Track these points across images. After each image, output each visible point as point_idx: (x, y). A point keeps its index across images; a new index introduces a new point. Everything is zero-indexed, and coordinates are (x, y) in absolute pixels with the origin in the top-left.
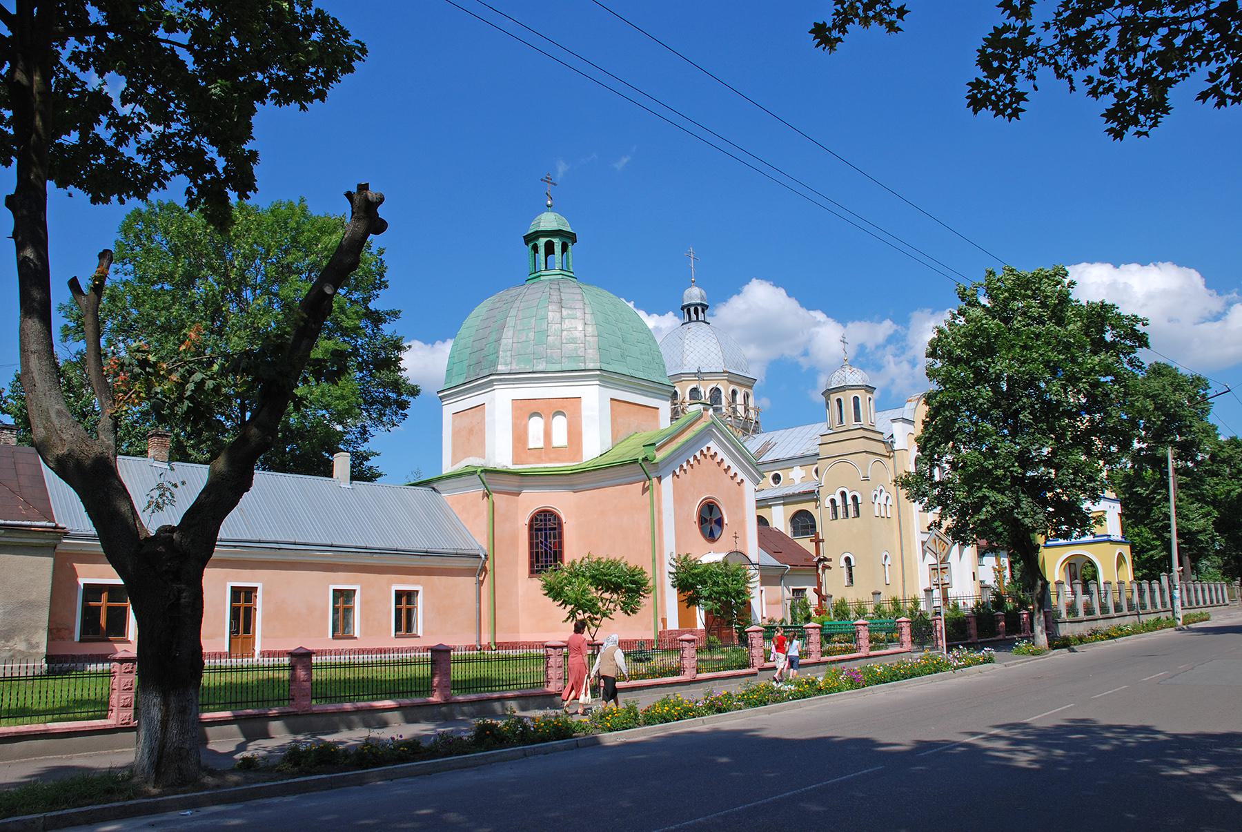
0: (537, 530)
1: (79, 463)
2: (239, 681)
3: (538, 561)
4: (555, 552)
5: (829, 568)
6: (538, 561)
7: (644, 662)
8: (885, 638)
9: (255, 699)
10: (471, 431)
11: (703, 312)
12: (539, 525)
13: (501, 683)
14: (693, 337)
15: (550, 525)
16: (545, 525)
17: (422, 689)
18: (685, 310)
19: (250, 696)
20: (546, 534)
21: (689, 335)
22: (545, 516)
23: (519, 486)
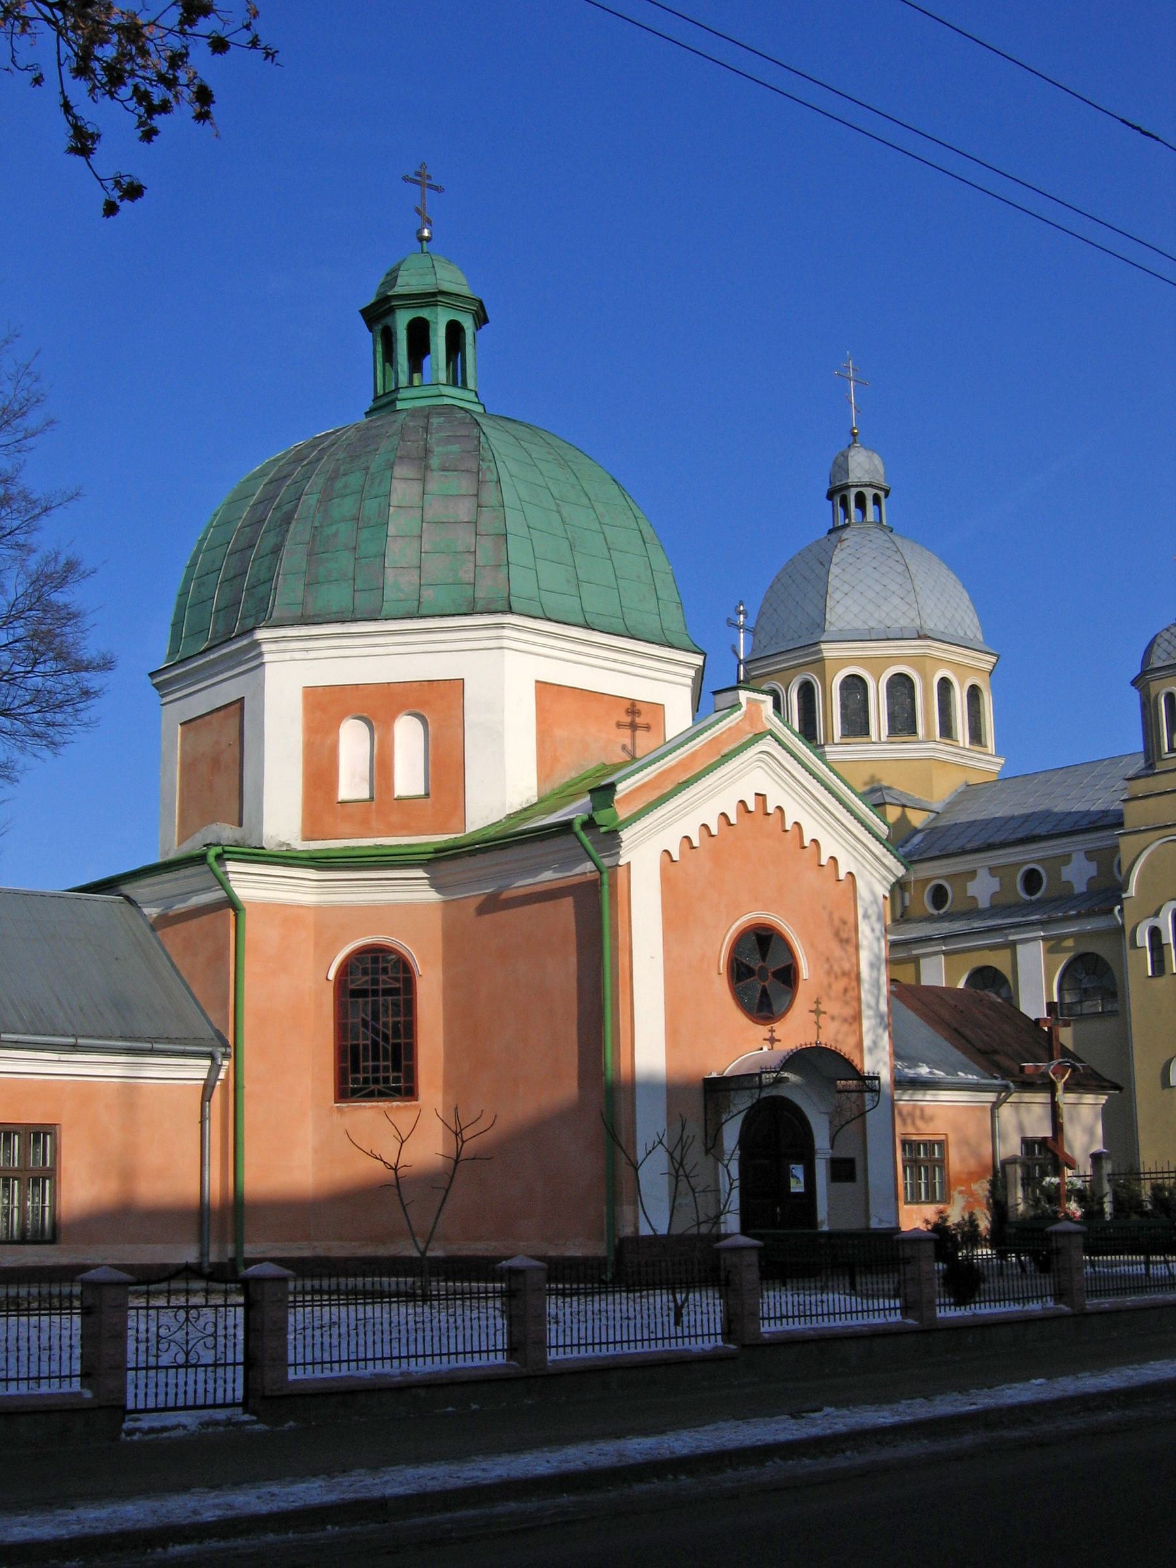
0: (356, 994)
1: (974, 1221)
2: (881, 1300)
3: (355, 1068)
4: (397, 1047)
5: (266, 59)
6: (355, 1068)
7: (28, 1312)
8: (1065, 1099)
9: (871, 1308)
10: (216, 763)
11: (877, 500)
12: (361, 981)
13: (1156, 1283)
14: (851, 559)
15: (385, 982)
16: (375, 982)
17: (1021, 1296)
18: (838, 499)
19: (412, 1347)
20: (375, 1003)
21: (843, 555)
22: (375, 960)
23: (779, 1081)
